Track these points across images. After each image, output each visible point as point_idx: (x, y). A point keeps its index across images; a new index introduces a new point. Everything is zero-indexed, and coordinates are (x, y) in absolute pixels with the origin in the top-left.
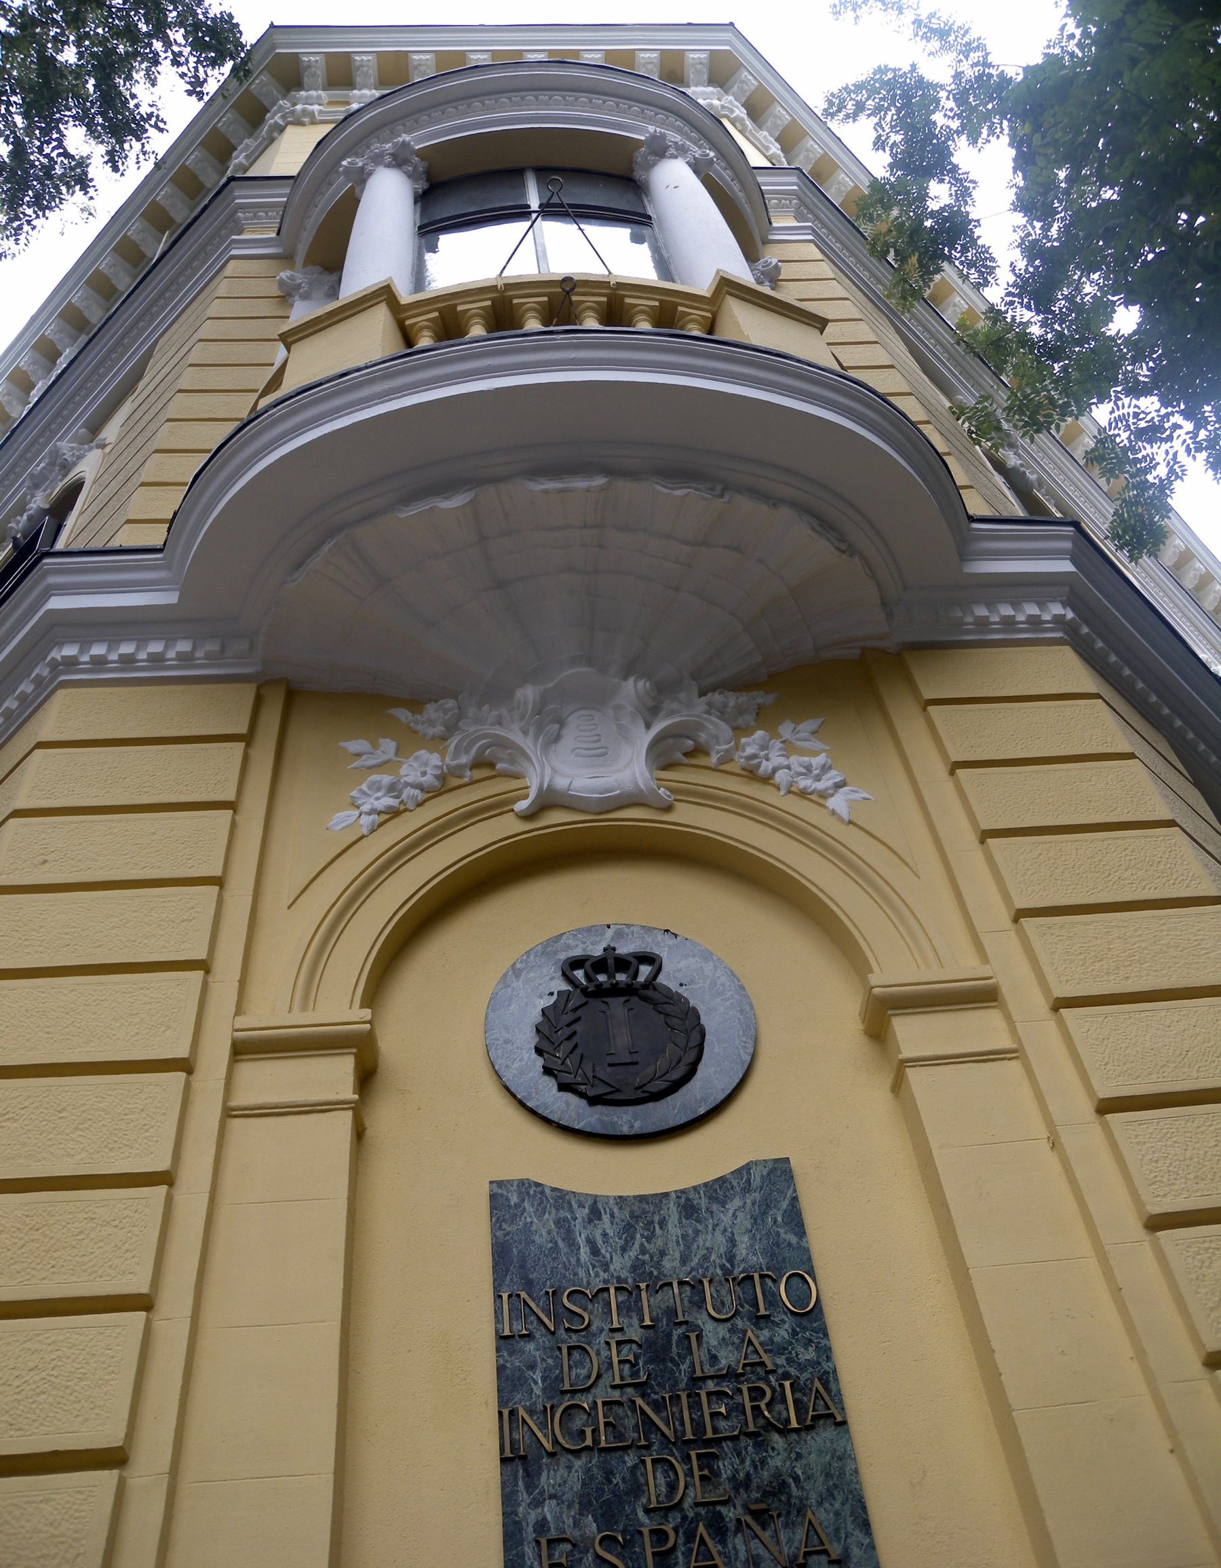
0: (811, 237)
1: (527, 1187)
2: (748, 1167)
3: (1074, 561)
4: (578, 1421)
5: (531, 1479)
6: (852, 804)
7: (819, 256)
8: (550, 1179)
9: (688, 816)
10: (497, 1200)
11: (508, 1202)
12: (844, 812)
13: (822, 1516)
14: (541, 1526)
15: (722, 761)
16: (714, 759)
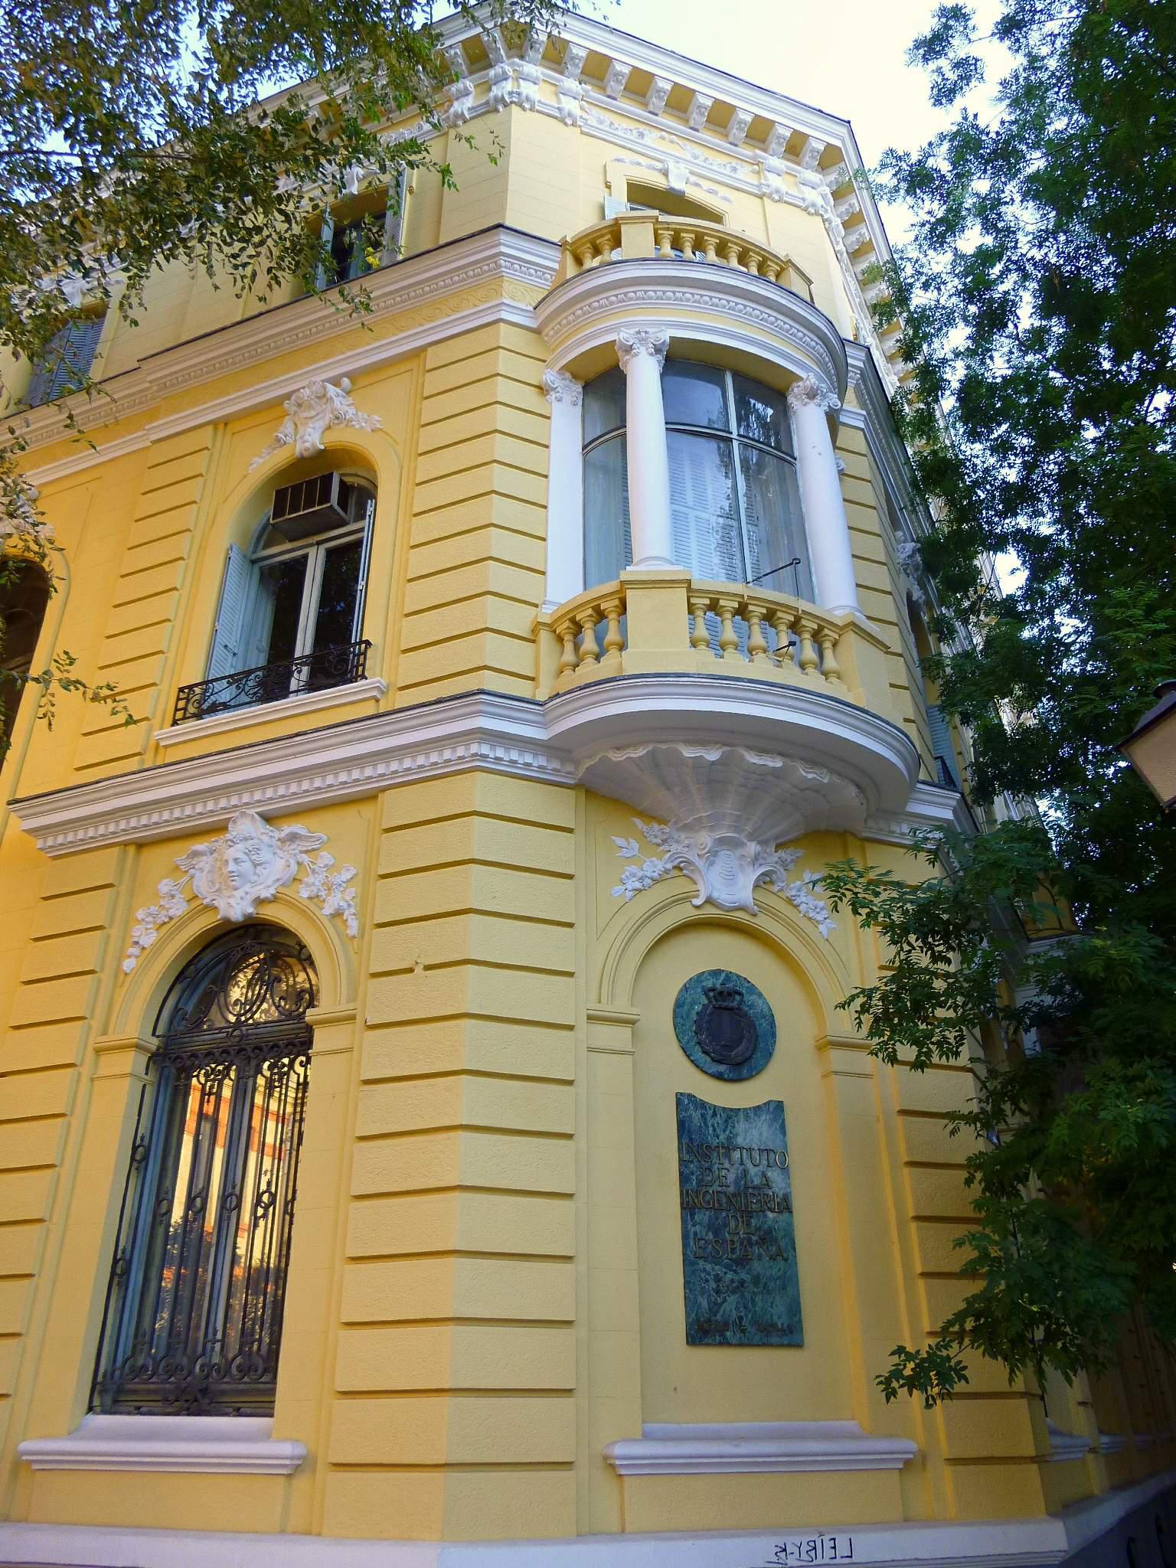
0: (862, 426)
1: (690, 1096)
2: (769, 1102)
3: (954, 812)
4: (708, 1197)
5: (692, 1215)
6: (829, 930)
7: (864, 449)
8: (700, 1095)
9: (764, 923)
10: (679, 1103)
11: (685, 1103)
12: (825, 933)
13: (782, 1244)
14: (695, 1233)
15: (781, 890)
16: (775, 889)
